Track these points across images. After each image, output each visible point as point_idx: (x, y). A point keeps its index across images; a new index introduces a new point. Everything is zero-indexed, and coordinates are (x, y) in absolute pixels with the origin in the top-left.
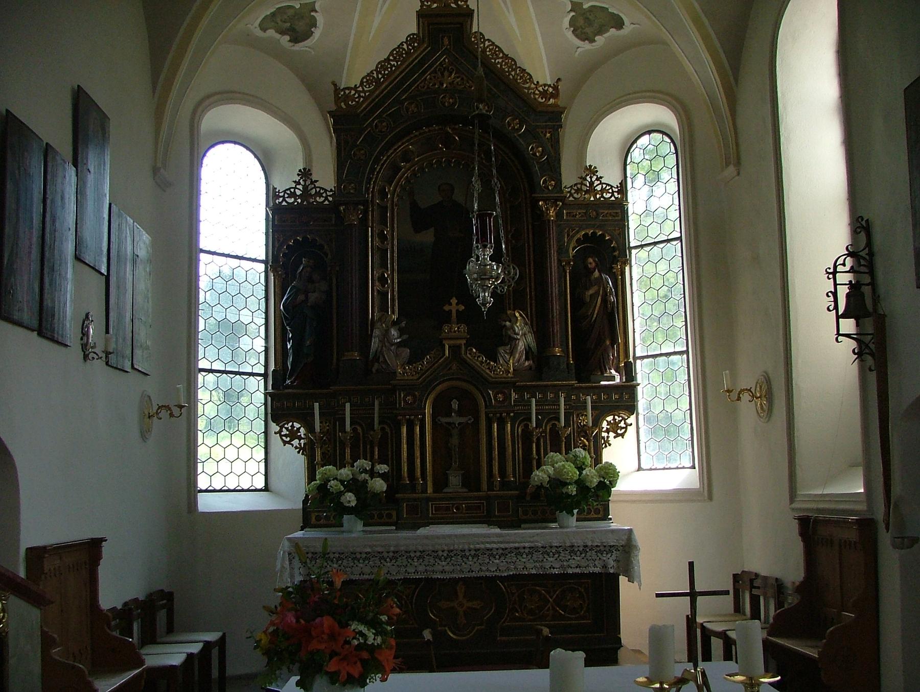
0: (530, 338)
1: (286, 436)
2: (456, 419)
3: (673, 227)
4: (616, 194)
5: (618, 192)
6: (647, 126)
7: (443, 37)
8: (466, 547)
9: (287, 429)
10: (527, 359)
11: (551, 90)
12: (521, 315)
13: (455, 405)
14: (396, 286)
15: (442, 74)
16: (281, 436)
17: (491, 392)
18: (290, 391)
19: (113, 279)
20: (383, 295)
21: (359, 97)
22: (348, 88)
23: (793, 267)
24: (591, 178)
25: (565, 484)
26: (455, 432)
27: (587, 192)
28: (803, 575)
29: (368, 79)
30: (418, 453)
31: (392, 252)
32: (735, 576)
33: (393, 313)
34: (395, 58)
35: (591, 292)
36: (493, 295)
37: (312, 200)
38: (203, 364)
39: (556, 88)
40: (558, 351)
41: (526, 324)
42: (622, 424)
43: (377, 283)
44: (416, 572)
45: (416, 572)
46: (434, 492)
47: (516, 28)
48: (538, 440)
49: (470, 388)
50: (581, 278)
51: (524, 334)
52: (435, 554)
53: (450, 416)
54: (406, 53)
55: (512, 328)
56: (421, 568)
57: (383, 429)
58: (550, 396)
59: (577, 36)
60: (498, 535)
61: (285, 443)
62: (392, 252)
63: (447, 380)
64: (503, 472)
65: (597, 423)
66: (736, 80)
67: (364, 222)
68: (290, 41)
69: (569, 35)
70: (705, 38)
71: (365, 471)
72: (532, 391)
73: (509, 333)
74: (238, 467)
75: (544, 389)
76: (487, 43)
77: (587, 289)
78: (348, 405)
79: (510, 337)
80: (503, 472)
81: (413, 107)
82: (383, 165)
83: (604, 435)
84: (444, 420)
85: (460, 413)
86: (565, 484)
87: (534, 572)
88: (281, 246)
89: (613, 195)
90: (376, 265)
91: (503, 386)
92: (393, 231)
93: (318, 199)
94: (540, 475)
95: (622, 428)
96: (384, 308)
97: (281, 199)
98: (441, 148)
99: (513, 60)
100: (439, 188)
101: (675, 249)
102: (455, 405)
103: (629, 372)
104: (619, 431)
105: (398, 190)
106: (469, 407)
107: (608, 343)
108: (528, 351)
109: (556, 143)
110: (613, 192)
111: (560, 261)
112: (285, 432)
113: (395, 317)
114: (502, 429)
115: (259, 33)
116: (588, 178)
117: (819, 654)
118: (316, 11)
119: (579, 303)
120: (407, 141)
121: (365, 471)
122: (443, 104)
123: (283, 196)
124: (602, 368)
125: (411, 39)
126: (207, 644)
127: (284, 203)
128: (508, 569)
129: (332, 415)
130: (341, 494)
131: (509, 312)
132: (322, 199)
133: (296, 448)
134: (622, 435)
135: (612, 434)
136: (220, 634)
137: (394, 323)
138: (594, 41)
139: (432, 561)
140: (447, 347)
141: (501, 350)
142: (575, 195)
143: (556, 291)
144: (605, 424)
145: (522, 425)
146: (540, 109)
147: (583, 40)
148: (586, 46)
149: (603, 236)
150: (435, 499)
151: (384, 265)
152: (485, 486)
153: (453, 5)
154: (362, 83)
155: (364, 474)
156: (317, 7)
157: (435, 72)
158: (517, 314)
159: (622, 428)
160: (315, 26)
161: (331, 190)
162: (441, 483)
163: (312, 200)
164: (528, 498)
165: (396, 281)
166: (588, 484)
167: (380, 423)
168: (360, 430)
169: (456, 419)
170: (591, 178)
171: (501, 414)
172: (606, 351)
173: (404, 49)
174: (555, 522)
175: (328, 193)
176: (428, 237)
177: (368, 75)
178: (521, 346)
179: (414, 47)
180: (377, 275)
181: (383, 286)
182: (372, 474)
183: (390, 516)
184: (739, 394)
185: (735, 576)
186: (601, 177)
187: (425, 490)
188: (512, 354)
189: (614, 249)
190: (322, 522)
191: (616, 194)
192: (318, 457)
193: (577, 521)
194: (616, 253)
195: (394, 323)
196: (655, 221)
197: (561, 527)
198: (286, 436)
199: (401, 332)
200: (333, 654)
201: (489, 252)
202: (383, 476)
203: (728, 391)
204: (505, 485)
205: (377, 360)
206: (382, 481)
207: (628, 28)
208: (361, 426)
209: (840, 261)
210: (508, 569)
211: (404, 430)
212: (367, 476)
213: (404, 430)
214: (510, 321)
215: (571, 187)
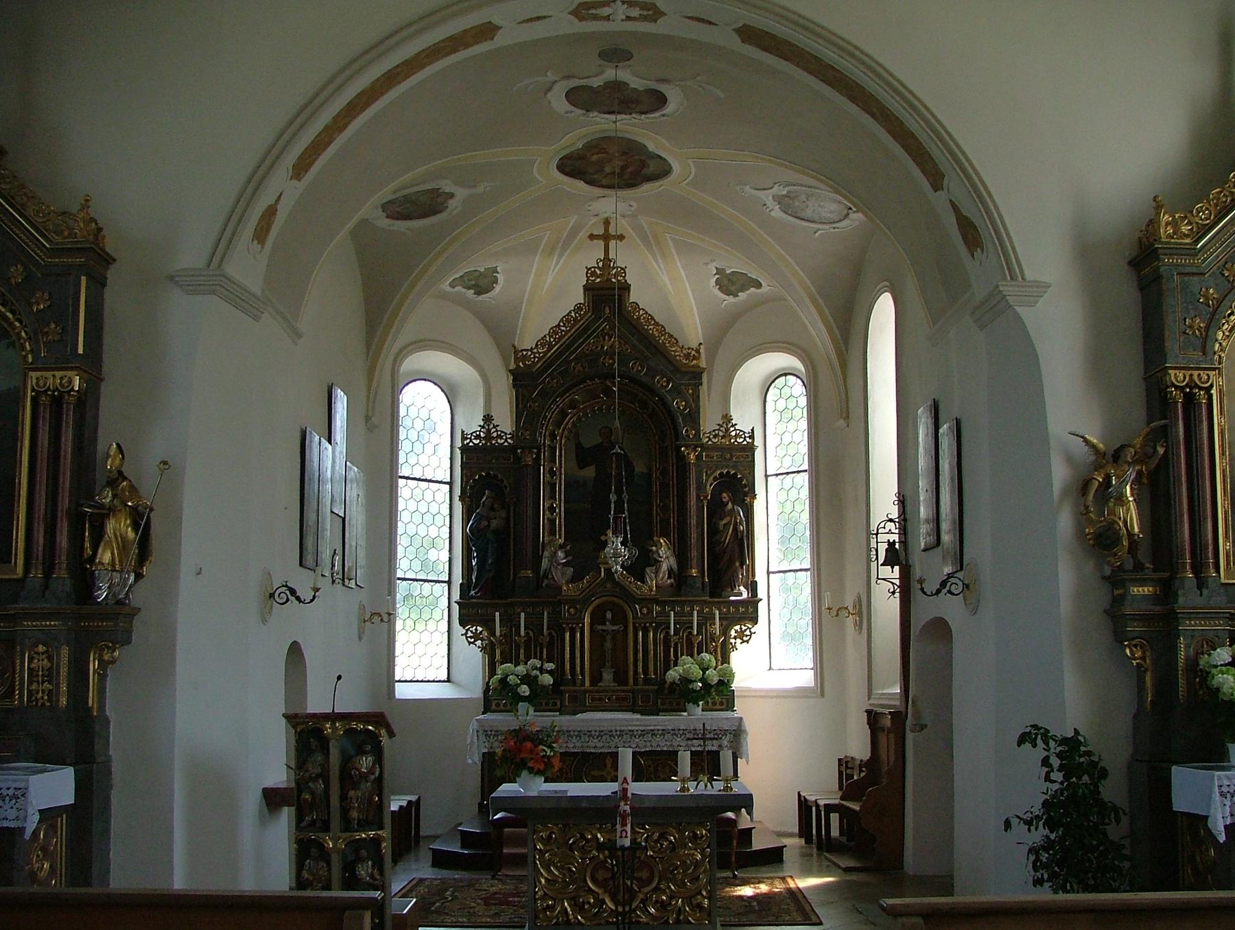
0: (673, 562)
1: (471, 637)
2: (609, 627)
4: (747, 439)
5: (750, 437)
6: (784, 369)
7: (605, 307)
8: (613, 728)
9: (472, 632)
10: (669, 577)
11: (693, 352)
12: (665, 541)
13: (609, 615)
14: (563, 514)
15: (604, 339)
16: (467, 637)
17: (637, 606)
18: (474, 600)
19: (347, 519)
20: (552, 522)
21: (535, 357)
22: (525, 350)
23: (874, 514)
24: (727, 425)
25: (691, 682)
26: (609, 638)
27: (723, 437)
28: (870, 755)
29: (542, 342)
30: (578, 654)
31: (560, 485)
32: (840, 760)
33: (560, 537)
34: (564, 324)
35: (724, 522)
36: (622, 566)
37: (494, 442)
38: (400, 574)
40: (694, 572)
41: (669, 549)
42: (747, 633)
43: (547, 513)
44: (574, 747)
45: (574, 747)
46: (591, 685)
47: (670, 286)
48: (676, 644)
50: (716, 508)
51: (667, 557)
52: (589, 734)
53: (605, 624)
54: (574, 321)
55: (657, 552)
56: (578, 744)
57: (550, 634)
58: (687, 609)
59: (722, 292)
60: (637, 720)
61: (470, 643)
62: (560, 485)
63: (604, 596)
64: (646, 671)
65: (725, 632)
66: (847, 350)
67: (537, 461)
68: (475, 294)
69: (716, 291)
70: (821, 313)
71: (536, 668)
72: (673, 604)
73: (655, 556)
74: (425, 662)
75: (682, 604)
76: (641, 312)
77: (722, 519)
78: (523, 615)
79: (656, 559)
80: (646, 671)
81: (579, 367)
82: (553, 412)
83: (732, 641)
84: (600, 627)
85: (613, 622)
86: (691, 682)
87: (665, 749)
88: (467, 482)
89: (745, 440)
90: (546, 534)
91: (646, 601)
92: (561, 467)
93: (499, 441)
94: (673, 674)
95: (747, 636)
96: (552, 532)
97: (468, 441)
98: (603, 398)
99: (663, 327)
100: (600, 432)
101: (805, 476)
102: (609, 615)
103: (753, 587)
104: (745, 639)
105: (566, 432)
106: (620, 617)
107: (737, 564)
108: (670, 571)
109: (696, 398)
110: (745, 437)
111: (698, 496)
112: (470, 634)
113: (561, 541)
114: (645, 637)
115: (449, 289)
116: (724, 425)
117: (861, 806)
118: (498, 272)
119: (714, 531)
120: (573, 393)
121: (536, 668)
122: (604, 364)
123: (470, 438)
124: (732, 586)
125: (578, 308)
126: (410, 802)
127: (471, 444)
128: (645, 747)
129: (510, 622)
130: (518, 686)
131: (655, 538)
132: (503, 441)
133: (479, 647)
134: (747, 642)
135: (739, 641)
136: (417, 797)
137: (561, 547)
138: (737, 296)
139: (587, 739)
140: (603, 570)
141: (648, 570)
142: (713, 440)
143: (694, 522)
144: (733, 633)
145: (664, 632)
146: (684, 369)
147: (728, 295)
148: (731, 299)
149: (735, 474)
150: (589, 691)
151: (553, 497)
152: (631, 681)
153: (613, 280)
154: (537, 345)
156: (498, 269)
157: (597, 336)
158: (662, 541)
159: (747, 636)
160: (496, 283)
161: (510, 434)
162: (596, 678)
163: (494, 442)
164: (666, 692)
165: (563, 509)
166: (709, 682)
167: (548, 629)
168: (531, 634)
169: (609, 627)
170: (727, 425)
171: (645, 624)
172: (736, 571)
173: (572, 317)
174: (685, 711)
175: (508, 436)
176: (590, 472)
177: (542, 339)
178: (664, 567)
179: (580, 314)
180: (547, 468)
181: (552, 515)
182: (541, 670)
183: (555, 704)
184: (838, 611)
185: (840, 760)
186: (736, 425)
187: (583, 684)
188: (657, 573)
189: (745, 486)
190: (500, 708)
191: (747, 439)
192: (498, 657)
193: (703, 711)
194: (746, 489)
195: (561, 547)
196: (788, 453)
197: (689, 715)
198: (471, 637)
199: (567, 554)
200: (532, 759)
201: (620, 539)
202: (550, 672)
203: (829, 609)
204: (647, 681)
205: (547, 577)
206: (549, 677)
207: (765, 288)
208: (532, 630)
209: (882, 525)
210: (645, 747)
211: (567, 635)
212: (538, 673)
213: (567, 635)
214: (656, 546)
215: (710, 433)
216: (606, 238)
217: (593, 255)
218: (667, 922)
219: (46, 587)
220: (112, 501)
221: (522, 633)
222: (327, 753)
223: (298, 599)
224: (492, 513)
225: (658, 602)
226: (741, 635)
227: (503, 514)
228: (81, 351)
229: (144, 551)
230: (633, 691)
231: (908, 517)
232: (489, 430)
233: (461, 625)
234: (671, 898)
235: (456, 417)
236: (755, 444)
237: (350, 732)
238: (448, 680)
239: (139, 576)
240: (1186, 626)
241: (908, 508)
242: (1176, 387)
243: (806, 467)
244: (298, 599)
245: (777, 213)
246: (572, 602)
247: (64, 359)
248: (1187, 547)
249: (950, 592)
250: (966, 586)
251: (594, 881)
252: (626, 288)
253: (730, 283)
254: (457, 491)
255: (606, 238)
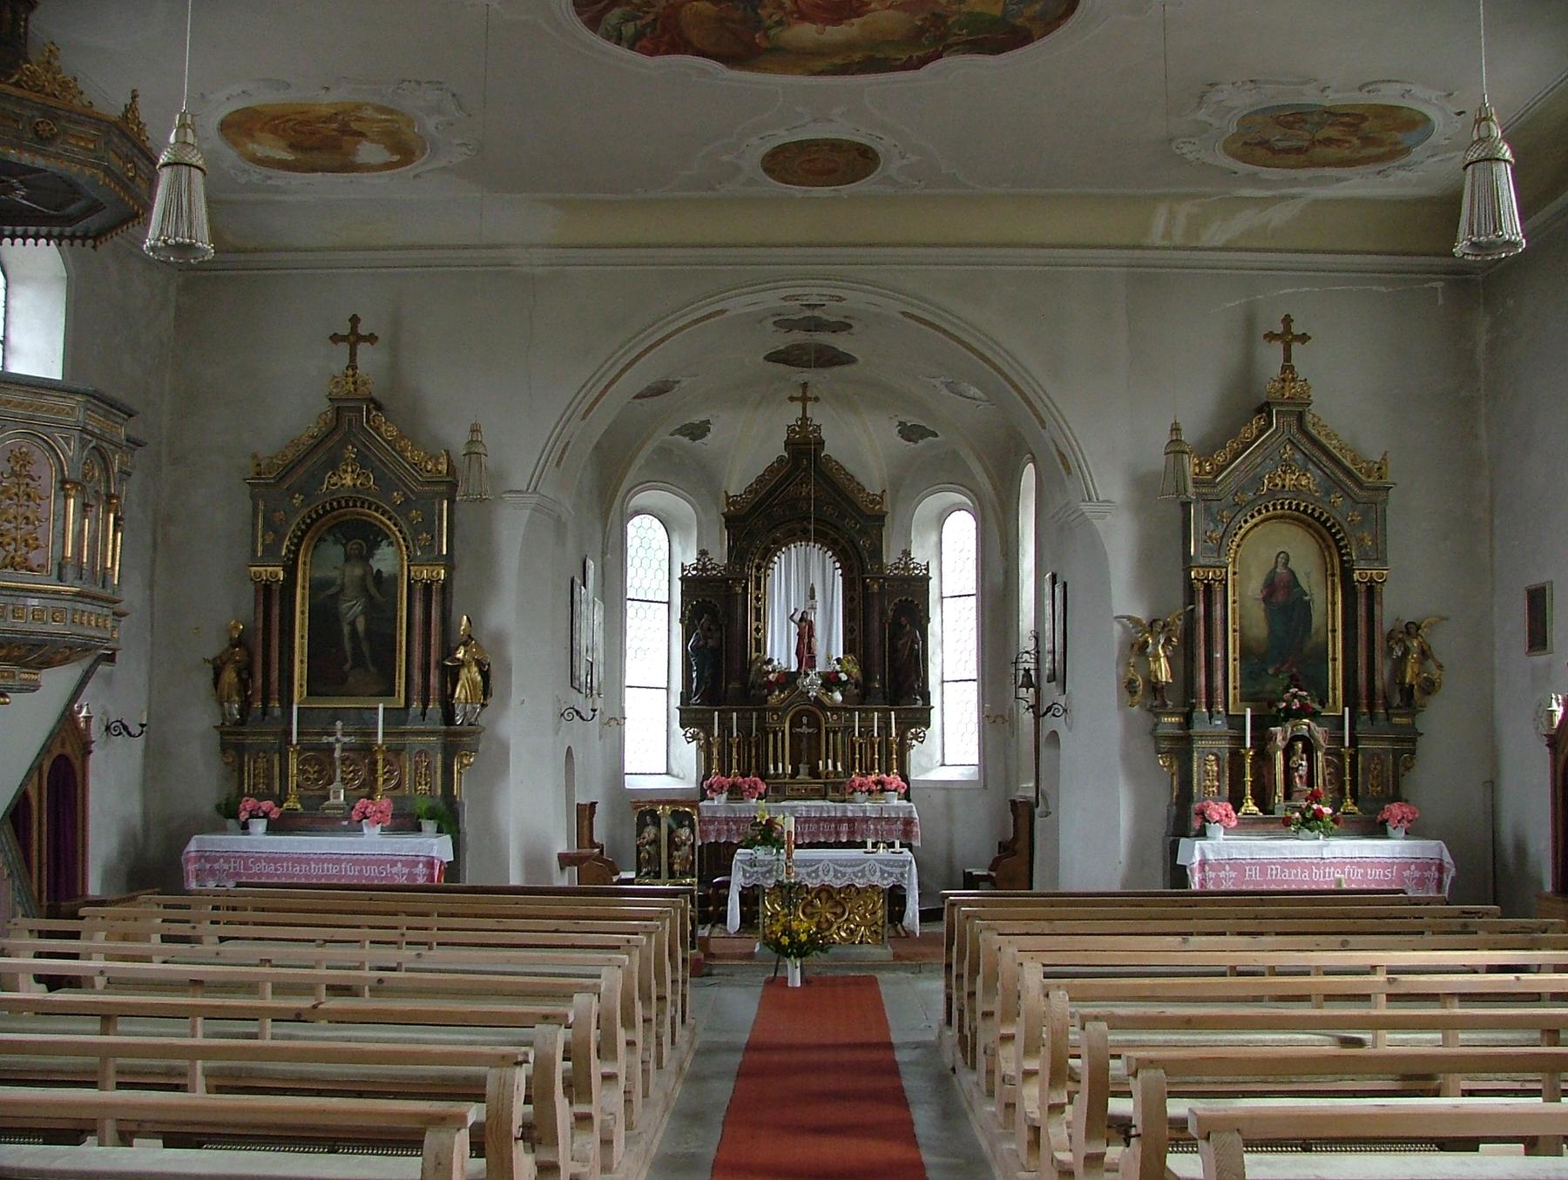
3: (970, 585)
13: (805, 720)
26: (805, 740)
29: (749, 490)
32: (1000, 843)
35: (901, 642)
39: (881, 497)
49: (818, 711)
53: (801, 727)
67: (746, 588)
75: (866, 711)
85: (808, 726)
101: (973, 599)
102: (805, 720)
111: (881, 621)
119: (894, 650)
125: (781, 459)
144: (910, 736)
155: (270, 803)
169: (805, 730)
180: (754, 596)
211: (771, 736)
213: (771, 736)
216: (804, 400)
217: (793, 413)
218: (854, 943)
219: (424, 714)
220: (464, 655)
221: (735, 735)
222: (659, 826)
223: (581, 717)
224: (709, 634)
225: (846, 709)
226: (916, 736)
227: (717, 635)
228: (445, 553)
229: (486, 691)
230: (825, 784)
231: (1040, 650)
232: (704, 563)
233: (681, 727)
234: (857, 926)
235: (672, 544)
236: (930, 575)
237: (674, 814)
238: (667, 774)
239: (483, 706)
240: (1198, 744)
241: (1040, 643)
242: (1198, 580)
243: (974, 592)
244: (581, 717)
245: (945, 392)
246: (775, 710)
247: (433, 562)
248: (1203, 691)
249: (1054, 715)
250: (1065, 711)
251: (804, 913)
252: (821, 443)
253: (910, 433)
254: (676, 614)
255: (804, 400)
